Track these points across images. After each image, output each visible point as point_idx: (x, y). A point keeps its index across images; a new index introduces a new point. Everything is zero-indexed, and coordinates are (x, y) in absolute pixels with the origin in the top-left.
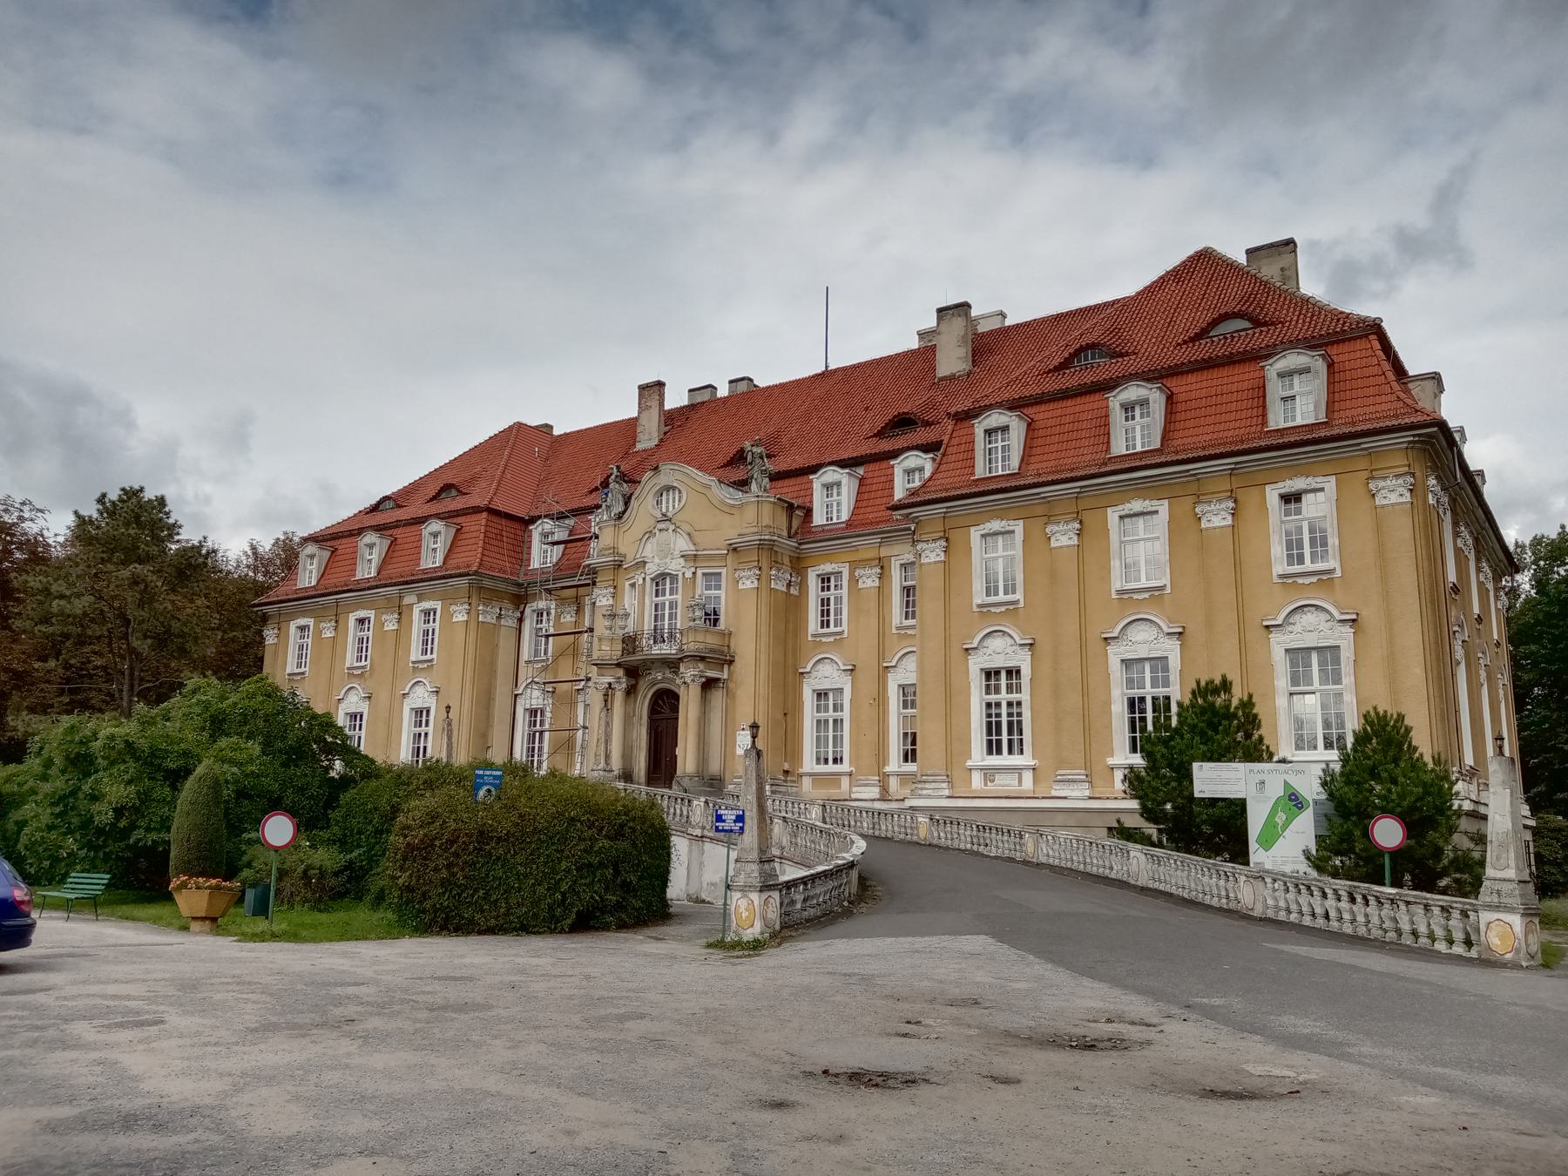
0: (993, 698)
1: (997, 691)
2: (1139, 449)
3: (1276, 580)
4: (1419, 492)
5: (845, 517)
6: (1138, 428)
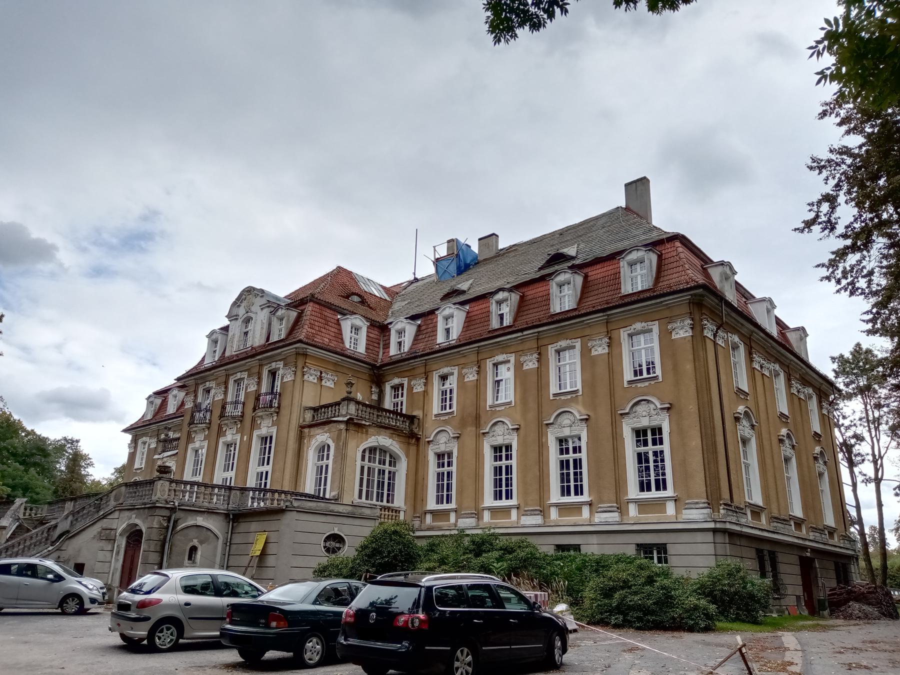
0: (642, 449)
2: (640, 289)
3: (626, 385)
4: (698, 328)
5: (406, 350)
6: (639, 277)
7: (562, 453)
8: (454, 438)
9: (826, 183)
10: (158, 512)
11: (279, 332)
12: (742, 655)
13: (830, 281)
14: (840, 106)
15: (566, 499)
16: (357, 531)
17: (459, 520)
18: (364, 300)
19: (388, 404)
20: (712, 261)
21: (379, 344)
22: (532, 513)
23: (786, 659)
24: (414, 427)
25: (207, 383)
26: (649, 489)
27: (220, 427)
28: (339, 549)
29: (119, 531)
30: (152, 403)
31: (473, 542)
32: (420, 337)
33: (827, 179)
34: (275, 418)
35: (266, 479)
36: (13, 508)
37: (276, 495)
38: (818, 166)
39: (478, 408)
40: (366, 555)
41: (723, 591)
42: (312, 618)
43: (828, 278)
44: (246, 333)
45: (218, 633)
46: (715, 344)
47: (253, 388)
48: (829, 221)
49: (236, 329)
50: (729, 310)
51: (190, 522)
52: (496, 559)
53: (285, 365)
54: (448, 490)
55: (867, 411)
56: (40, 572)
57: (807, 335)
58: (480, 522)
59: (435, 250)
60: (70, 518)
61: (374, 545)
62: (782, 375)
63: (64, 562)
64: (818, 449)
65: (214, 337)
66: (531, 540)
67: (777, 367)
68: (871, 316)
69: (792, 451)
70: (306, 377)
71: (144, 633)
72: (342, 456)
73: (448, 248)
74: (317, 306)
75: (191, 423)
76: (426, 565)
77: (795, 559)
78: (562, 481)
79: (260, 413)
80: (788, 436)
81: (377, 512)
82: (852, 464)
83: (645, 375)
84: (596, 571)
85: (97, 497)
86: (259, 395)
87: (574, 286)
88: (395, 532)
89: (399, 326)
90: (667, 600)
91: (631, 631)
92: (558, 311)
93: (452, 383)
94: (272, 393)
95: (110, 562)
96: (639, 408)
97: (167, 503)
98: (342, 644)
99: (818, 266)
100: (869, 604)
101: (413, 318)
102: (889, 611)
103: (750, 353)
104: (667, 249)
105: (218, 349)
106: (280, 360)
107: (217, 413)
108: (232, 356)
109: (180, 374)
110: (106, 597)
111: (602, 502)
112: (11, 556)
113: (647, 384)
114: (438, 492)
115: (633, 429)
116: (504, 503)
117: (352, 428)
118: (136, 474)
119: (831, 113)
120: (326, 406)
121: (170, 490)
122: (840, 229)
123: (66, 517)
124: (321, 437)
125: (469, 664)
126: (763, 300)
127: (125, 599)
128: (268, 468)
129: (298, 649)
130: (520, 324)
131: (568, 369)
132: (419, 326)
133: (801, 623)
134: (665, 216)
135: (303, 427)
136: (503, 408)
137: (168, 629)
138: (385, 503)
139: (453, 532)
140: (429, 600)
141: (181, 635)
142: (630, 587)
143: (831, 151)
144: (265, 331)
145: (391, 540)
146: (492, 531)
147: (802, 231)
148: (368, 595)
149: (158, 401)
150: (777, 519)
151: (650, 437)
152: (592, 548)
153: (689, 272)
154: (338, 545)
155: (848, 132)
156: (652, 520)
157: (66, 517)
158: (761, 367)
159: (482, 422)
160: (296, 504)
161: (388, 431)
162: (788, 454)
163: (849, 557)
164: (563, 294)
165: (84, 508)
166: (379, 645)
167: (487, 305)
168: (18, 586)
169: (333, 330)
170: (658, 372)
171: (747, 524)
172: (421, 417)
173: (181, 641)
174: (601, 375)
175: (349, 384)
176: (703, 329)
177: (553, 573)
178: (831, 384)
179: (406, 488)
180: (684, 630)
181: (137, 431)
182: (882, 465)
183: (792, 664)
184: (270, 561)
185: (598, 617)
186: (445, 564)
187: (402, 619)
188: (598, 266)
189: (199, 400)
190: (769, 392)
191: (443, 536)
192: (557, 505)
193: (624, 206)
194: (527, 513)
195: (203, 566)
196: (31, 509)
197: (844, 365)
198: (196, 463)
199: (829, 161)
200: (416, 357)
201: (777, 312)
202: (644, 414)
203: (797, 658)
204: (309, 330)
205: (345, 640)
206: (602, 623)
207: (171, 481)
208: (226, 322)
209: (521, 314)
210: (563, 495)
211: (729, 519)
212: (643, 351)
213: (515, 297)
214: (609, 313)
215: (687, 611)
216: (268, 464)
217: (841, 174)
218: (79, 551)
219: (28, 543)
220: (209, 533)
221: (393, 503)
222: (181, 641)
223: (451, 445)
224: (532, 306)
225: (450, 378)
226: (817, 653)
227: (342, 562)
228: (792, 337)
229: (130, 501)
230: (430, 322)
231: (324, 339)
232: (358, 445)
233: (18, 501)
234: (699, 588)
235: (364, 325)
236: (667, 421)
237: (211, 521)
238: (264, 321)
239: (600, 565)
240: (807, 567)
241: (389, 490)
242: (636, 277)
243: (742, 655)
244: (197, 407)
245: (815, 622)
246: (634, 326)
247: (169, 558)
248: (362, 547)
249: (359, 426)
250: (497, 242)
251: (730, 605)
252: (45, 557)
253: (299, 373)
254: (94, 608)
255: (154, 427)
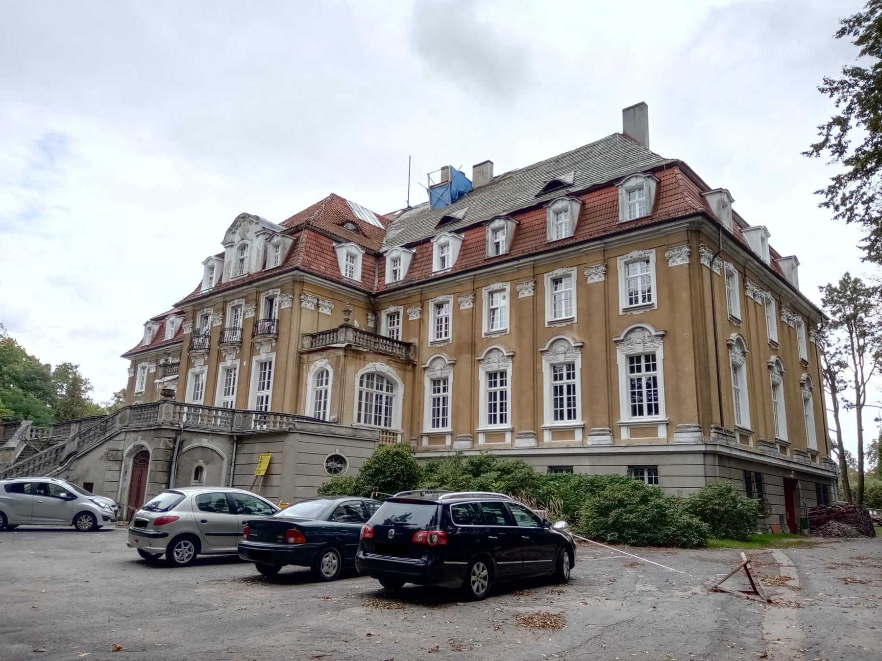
1: (639, 370)
2: (638, 216)
4: (695, 256)
5: (401, 279)
6: (637, 205)
7: (556, 379)
8: (450, 364)
9: (837, 106)
10: (164, 434)
11: (275, 260)
14: (860, 24)
15: (559, 423)
16: (357, 452)
17: (455, 443)
18: (359, 229)
19: (384, 332)
20: (709, 189)
21: (374, 272)
22: (525, 436)
23: (783, 574)
24: (410, 354)
26: (641, 413)
28: (341, 469)
29: (126, 452)
30: (150, 329)
31: (472, 463)
32: (416, 265)
34: (274, 344)
35: (267, 403)
36: (20, 429)
37: (278, 418)
38: (830, 87)
39: (473, 336)
40: (369, 475)
42: (328, 533)
43: (827, 205)
44: (242, 260)
45: (236, 549)
47: (251, 315)
48: (840, 144)
49: (232, 256)
50: (725, 238)
51: (195, 444)
52: (495, 479)
53: (282, 292)
54: (443, 415)
55: (852, 338)
56: (52, 490)
57: (798, 264)
58: (475, 445)
59: (429, 178)
60: (77, 439)
61: (377, 466)
62: (773, 303)
63: (73, 481)
64: (804, 376)
65: (210, 263)
66: (527, 461)
67: (769, 295)
68: (868, 243)
69: (780, 378)
70: (303, 304)
72: (341, 381)
73: (442, 175)
74: (312, 233)
75: (191, 349)
76: (428, 484)
77: (780, 481)
79: (258, 339)
80: (777, 363)
81: (377, 435)
82: (834, 390)
83: (640, 303)
84: (592, 491)
85: (100, 423)
86: (257, 322)
87: (572, 213)
89: (395, 254)
90: (661, 518)
91: (627, 547)
92: (555, 239)
93: (447, 311)
94: (270, 320)
95: (118, 482)
97: (172, 425)
99: (817, 192)
101: (409, 246)
102: (867, 530)
103: (744, 281)
106: (277, 287)
107: (216, 338)
108: (229, 283)
109: (178, 301)
110: (118, 515)
111: (594, 425)
112: (21, 476)
113: (642, 311)
114: (434, 416)
115: (627, 356)
116: (498, 426)
117: (350, 354)
118: (137, 398)
119: (850, 32)
120: (323, 333)
121: (174, 413)
122: (850, 153)
123: (73, 439)
124: (320, 363)
125: (485, 578)
126: (758, 229)
127: (142, 516)
128: (268, 392)
129: (316, 564)
130: (516, 253)
131: (563, 298)
132: (415, 255)
133: (786, 540)
134: (663, 145)
135: (302, 353)
136: (498, 336)
137: (186, 545)
138: (382, 426)
139: (451, 454)
141: (198, 550)
142: (625, 506)
143: (845, 72)
144: (261, 259)
145: (393, 461)
146: (490, 453)
148: (384, 512)
149: (156, 327)
151: (643, 364)
152: (585, 469)
153: (688, 199)
155: (863, 52)
156: (643, 442)
157: (73, 439)
158: (754, 295)
159: (477, 349)
160: (298, 426)
161: (385, 358)
162: (776, 380)
163: (829, 479)
164: (559, 222)
165: (90, 430)
167: (544, 215)
168: (33, 504)
169: (329, 257)
170: (654, 300)
171: (736, 447)
172: (417, 344)
173: (198, 556)
174: (597, 304)
175: (347, 312)
176: (700, 257)
177: (549, 493)
178: (820, 313)
179: (403, 413)
180: (678, 547)
181: (136, 356)
182: (864, 391)
183: (790, 578)
184: (275, 480)
185: (594, 534)
186: (445, 483)
187: (420, 535)
188: (596, 193)
189: (198, 326)
190: (761, 318)
191: (441, 457)
192: (550, 429)
193: (621, 132)
194: (521, 436)
196: (37, 431)
197: (833, 295)
198: (197, 387)
199: (842, 83)
200: (412, 285)
201: (771, 242)
202: (639, 341)
203: (793, 573)
204: (305, 257)
205: (364, 554)
206: (600, 539)
208: (221, 249)
209: (517, 243)
211: (719, 442)
212: (639, 279)
213: (511, 225)
214: (606, 240)
215: (680, 528)
216: (268, 388)
217: (854, 97)
219: (37, 463)
220: (214, 454)
221: (390, 426)
222: (198, 556)
223: (447, 371)
224: (528, 235)
225: (446, 306)
226: (811, 569)
227: (345, 482)
228: (784, 266)
229: (135, 424)
230: (425, 250)
231: (320, 267)
232: (357, 371)
233: (25, 423)
234: (690, 508)
235: (359, 253)
236: (661, 347)
239: (594, 486)
240: (789, 487)
241: (386, 414)
242: (634, 205)
244: (196, 333)
246: (631, 254)
248: (365, 467)
251: (719, 523)
252: (56, 476)
253: (296, 301)
254: (106, 526)
255: (153, 352)
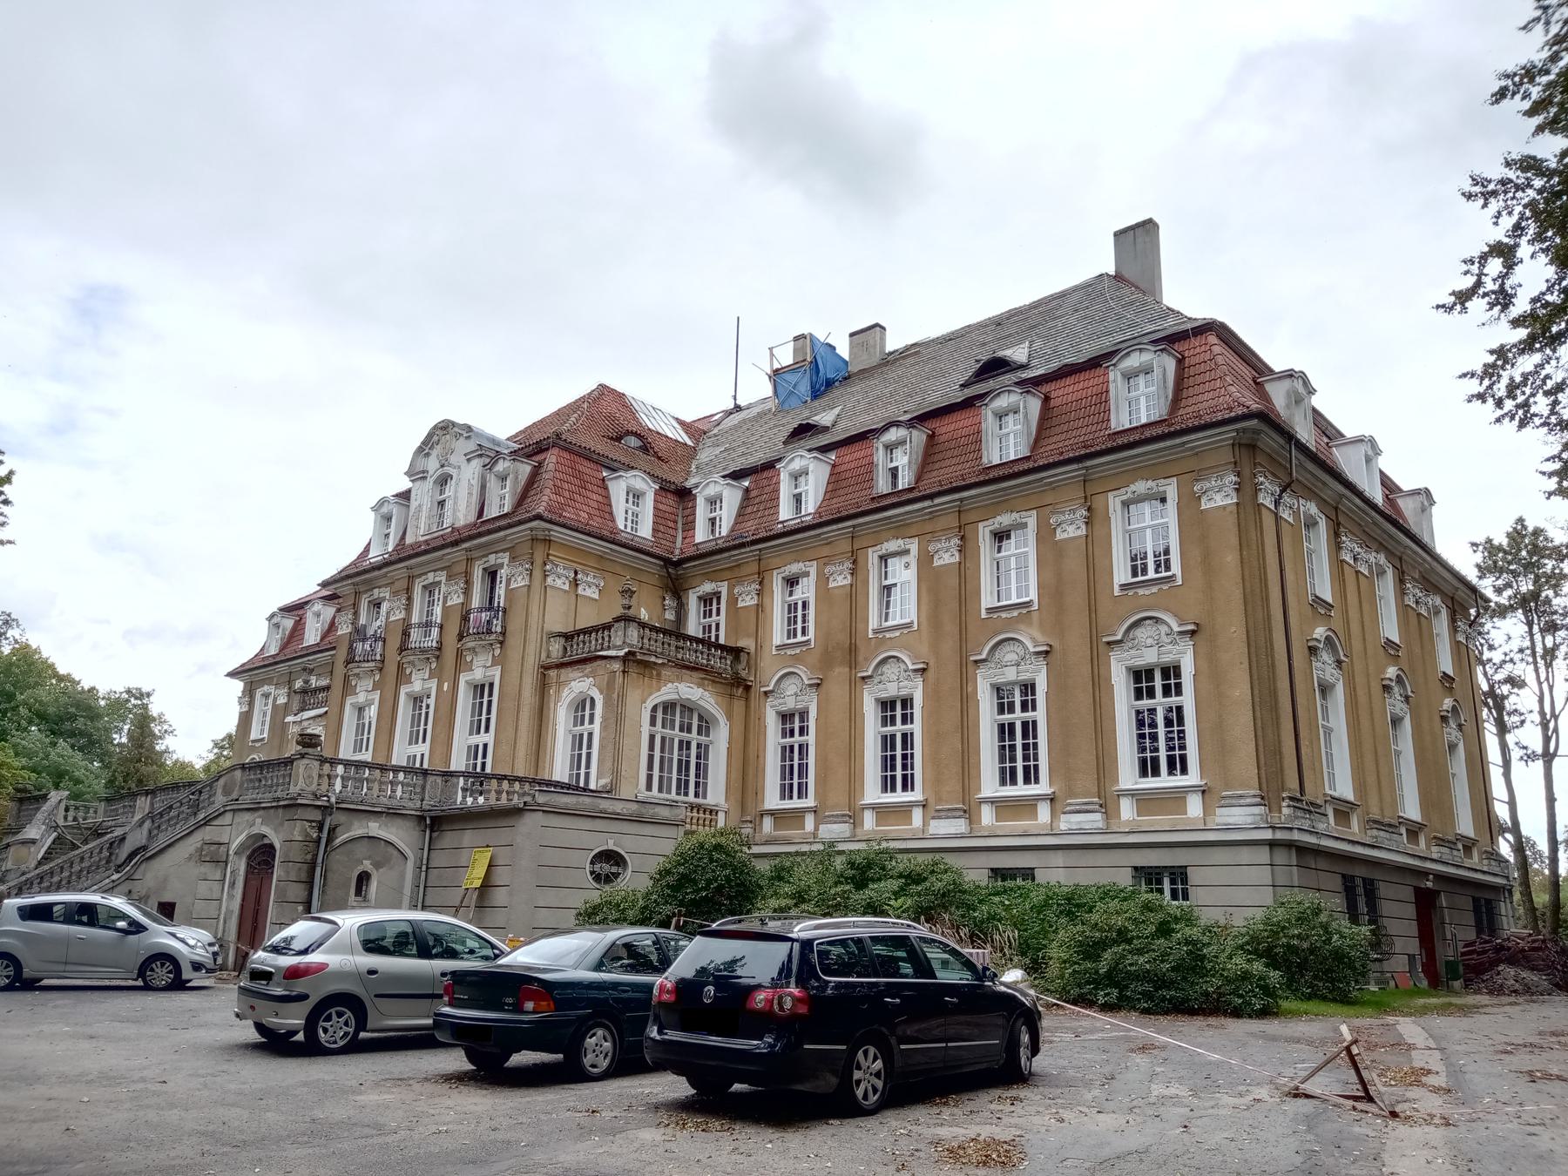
0: (1007, 717)
2: (1144, 421)
4: (1248, 489)
5: (724, 533)
6: (1143, 400)
9: (1496, 224)
10: (300, 813)
11: (500, 502)
12: (1351, 1057)
13: (1484, 402)
14: (1532, 80)
15: (1009, 791)
18: (648, 446)
19: (693, 627)
21: (675, 522)
22: (949, 814)
23: (1417, 1064)
24: (740, 667)
25: (376, 591)
27: (400, 667)
28: (617, 875)
29: (234, 846)
30: (277, 626)
31: (852, 864)
32: (749, 510)
33: (1498, 215)
34: (497, 652)
35: (484, 756)
36: (46, 807)
38: (1483, 190)
39: (852, 633)
40: (668, 886)
41: (1289, 947)
42: (594, 994)
43: (1481, 397)
44: (441, 504)
45: (430, 1021)
46: (1277, 518)
47: (456, 600)
48: (1502, 290)
49: (424, 496)
50: (1302, 458)
51: (357, 831)
52: (895, 893)
53: (513, 559)
56: (102, 916)
57: (1432, 503)
58: (858, 831)
59: (772, 355)
60: (148, 824)
61: (681, 869)
63: (139, 900)
64: (1448, 703)
65: (385, 510)
66: (952, 860)
67: (1382, 559)
70: (549, 580)
71: (299, 1022)
72: (616, 718)
73: (795, 351)
74: (567, 455)
75: (349, 661)
76: (774, 903)
77: (1409, 894)
78: (1002, 760)
80: (1399, 680)
81: (682, 813)
82: (1502, 729)
83: (1151, 574)
84: (1069, 913)
85: (188, 795)
86: (468, 612)
87: (1026, 415)
88: (718, 847)
89: (711, 491)
90: (1195, 962)
92: (996, 461)
93: (806, 590)
95: (220, 900)
96: (1142, 633)
97: (317, 797)
98: (653, 1040)
99: (1465, 375)
100: (1533, 969)
101: (736, 476)
103: (1337, 535)
104: (1193, 347)
105: (392, 530)
106: (504, 551)
107: (394, 642)
108: (419, 544)
110: (220, 961)
111: (1072, 795)
112: (48, 890)
113: (1154, 589)
115: (1129, 669)
116: (899, 797)
117: (633, 669)
118: (253, 749)
120: (586, 631)
121: (320, 776)
122: (1521, 306)
124: (579, 684)
125: (878, 1075)
127: (262, 963)
128: (488, 738)
129: (574, 1050)
130: (928, 486)
131: (1013, 565)
132: (747, 490)
133: (1421, 1001)
134: (1187, 293)
135: (547, 668)
137: (340, 1015)
138: (691, 798)
139: (815, 848)
140: (807, 963)
141: (361, 1024)
142: (1129, 941)
143: (1508, 164)
146: (884, 845)
147: (1449, 309)
148: (696, 955)
149: (289, 623)
150: (1378, 824)
151: (1158, 683)
152: (1055, 874)
153: (1232, 389)
154: (614, 869)
155: (1540, 129)
156: (1160, 824)
157: (141, 823)
158: (1355, 559)
159: (861, 658)
160: (541, 799)
161: (695, 674)
162: (1397, 711)
164: (1004, 431)
165: (171, 807)
166: (715, 1041)
168: (68, 941)
169: (595, 497)
170: (1176, 568)
171: (1327, 833)
172: (752, 650)
173: (363, 1035)
174: (1075, 578)
176: (1257, 491)
177: (992, 917)
178: (1474, 590)
180: (1225, 1014)
181: (252, 674)
182: (1556, 730)
183: (1429, 1072)
184: (499, 896)
185: (1075, 992)
186: (804, 901)
187: (761, 996)
188: (1069, 381)
190: (1368, 601)
191: (797, 853)
195: (380, 906)
196: (77, 808)
197: (1495, 558)
198: (360, 729)
199: (1503, 182)
200: (742, 545)
202: (1149, 641)
203: (1434, 1061)
204: (554, 497)
205: (660, 1032)
206: (1084, 1001)
207: (323, 761)
208: (405, 484)
209: (930, 467)
210: (1003, 783)
211: (1297, 824)
212: (1149, 531)
213: (919, 437)
214: (1089, 463)
215: (1228, 981)
216: (487, 730)
217: (1525, 206)
218: (166, 880)
219: (76, 868)
220: (390, 849)
221: (705, 797)
222: (363, 1035)
224: (949, 454)
225: (804, 581)
226: (1467, 1054)
227: (625, 899)
228: (1407, 507)
229: (250, 796)
233: (55, 796)
234: (1247, 943)
235: (649, 489)
237: (394, 830)
238: (474, 482)
239: (1073, 905)
240: (1425, 903)
241: (697, 776)
242: (1137, 400)
243: (1351, 1057)
244: (359, 633)
245: (1447, 1000)
246: (1132, 487)
247: (323, 892)
248: (660, 873)
249: (646, 665)
250: (883, 339)
251: (1302, 971)
252: (109, 890)
253: (537, 573)
